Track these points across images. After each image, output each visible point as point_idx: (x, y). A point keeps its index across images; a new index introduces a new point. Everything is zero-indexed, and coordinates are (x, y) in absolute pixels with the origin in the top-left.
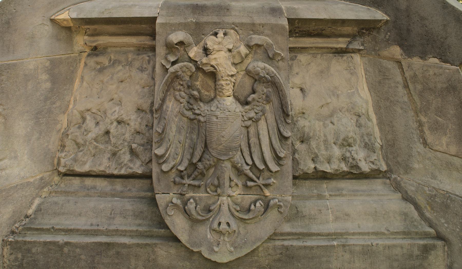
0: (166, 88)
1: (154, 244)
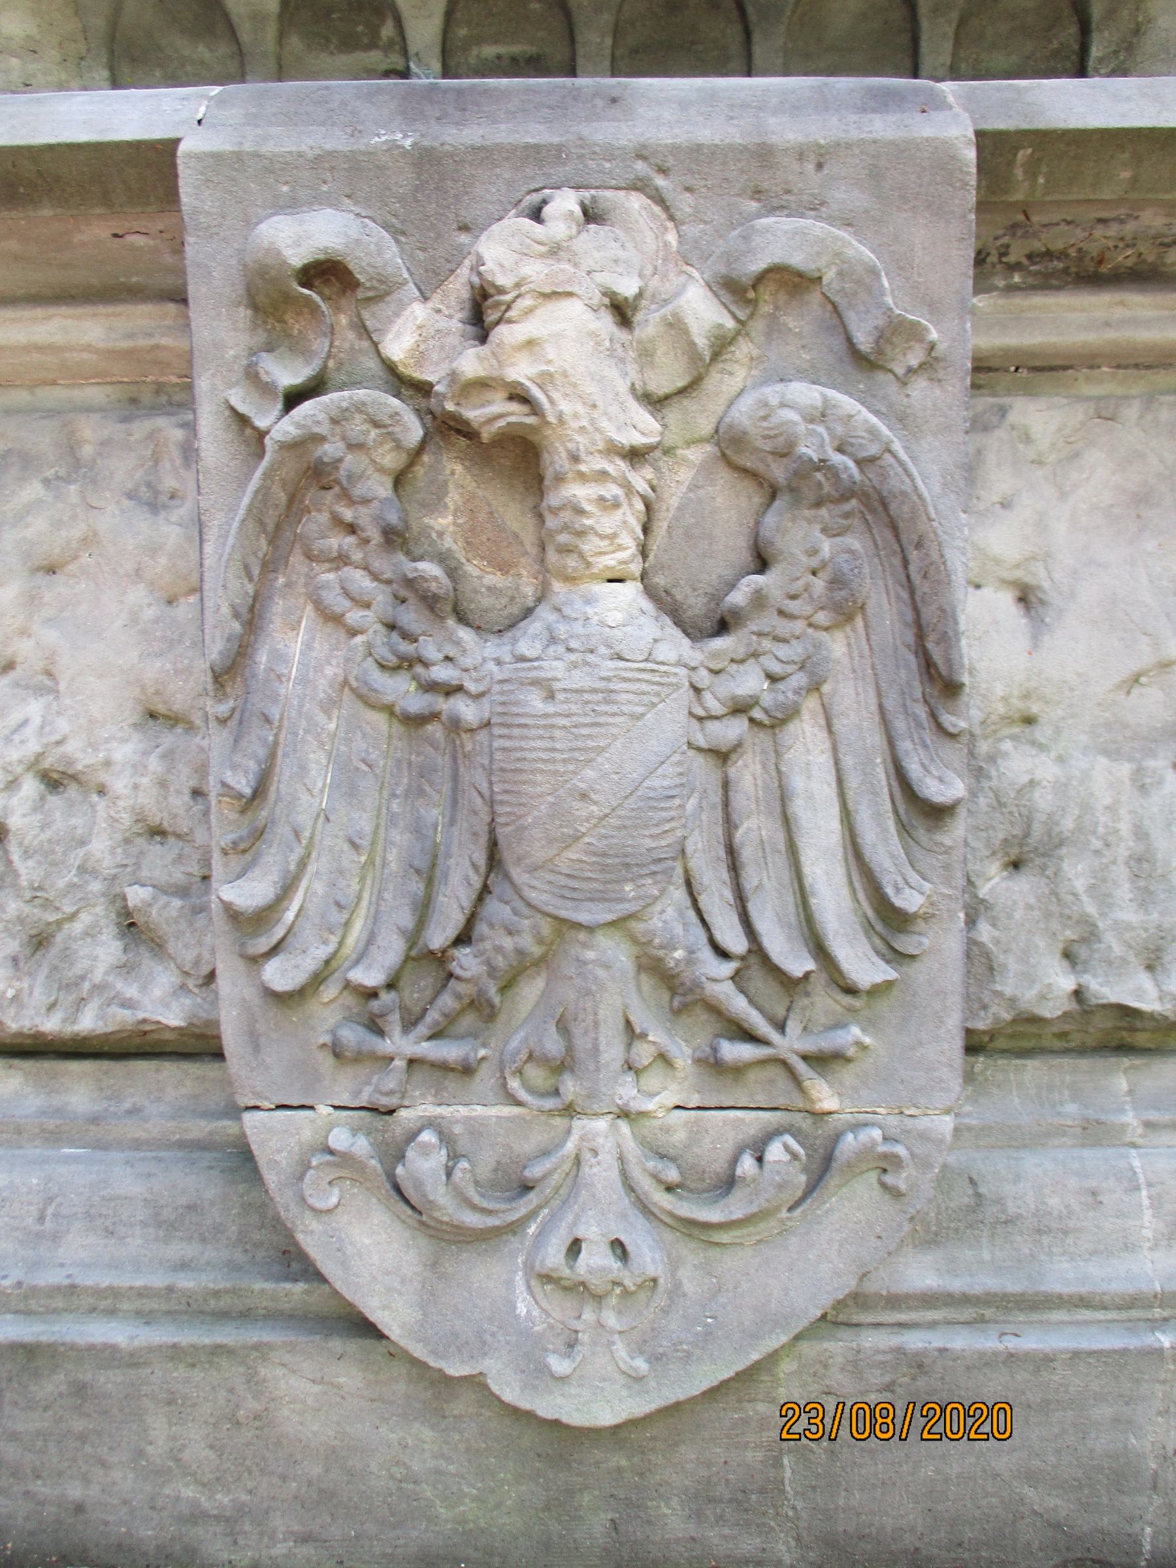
0: (263, 542)
1: (256, 1347)
